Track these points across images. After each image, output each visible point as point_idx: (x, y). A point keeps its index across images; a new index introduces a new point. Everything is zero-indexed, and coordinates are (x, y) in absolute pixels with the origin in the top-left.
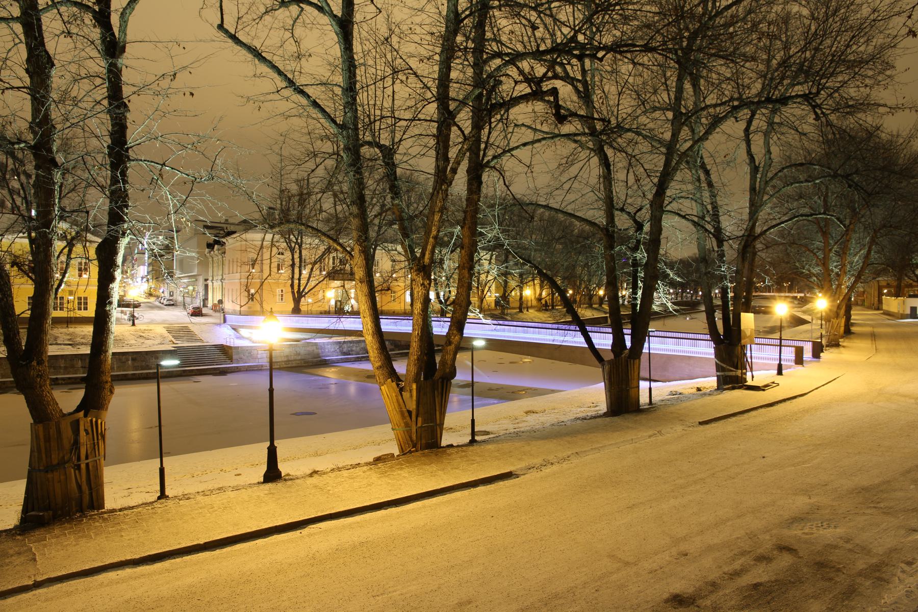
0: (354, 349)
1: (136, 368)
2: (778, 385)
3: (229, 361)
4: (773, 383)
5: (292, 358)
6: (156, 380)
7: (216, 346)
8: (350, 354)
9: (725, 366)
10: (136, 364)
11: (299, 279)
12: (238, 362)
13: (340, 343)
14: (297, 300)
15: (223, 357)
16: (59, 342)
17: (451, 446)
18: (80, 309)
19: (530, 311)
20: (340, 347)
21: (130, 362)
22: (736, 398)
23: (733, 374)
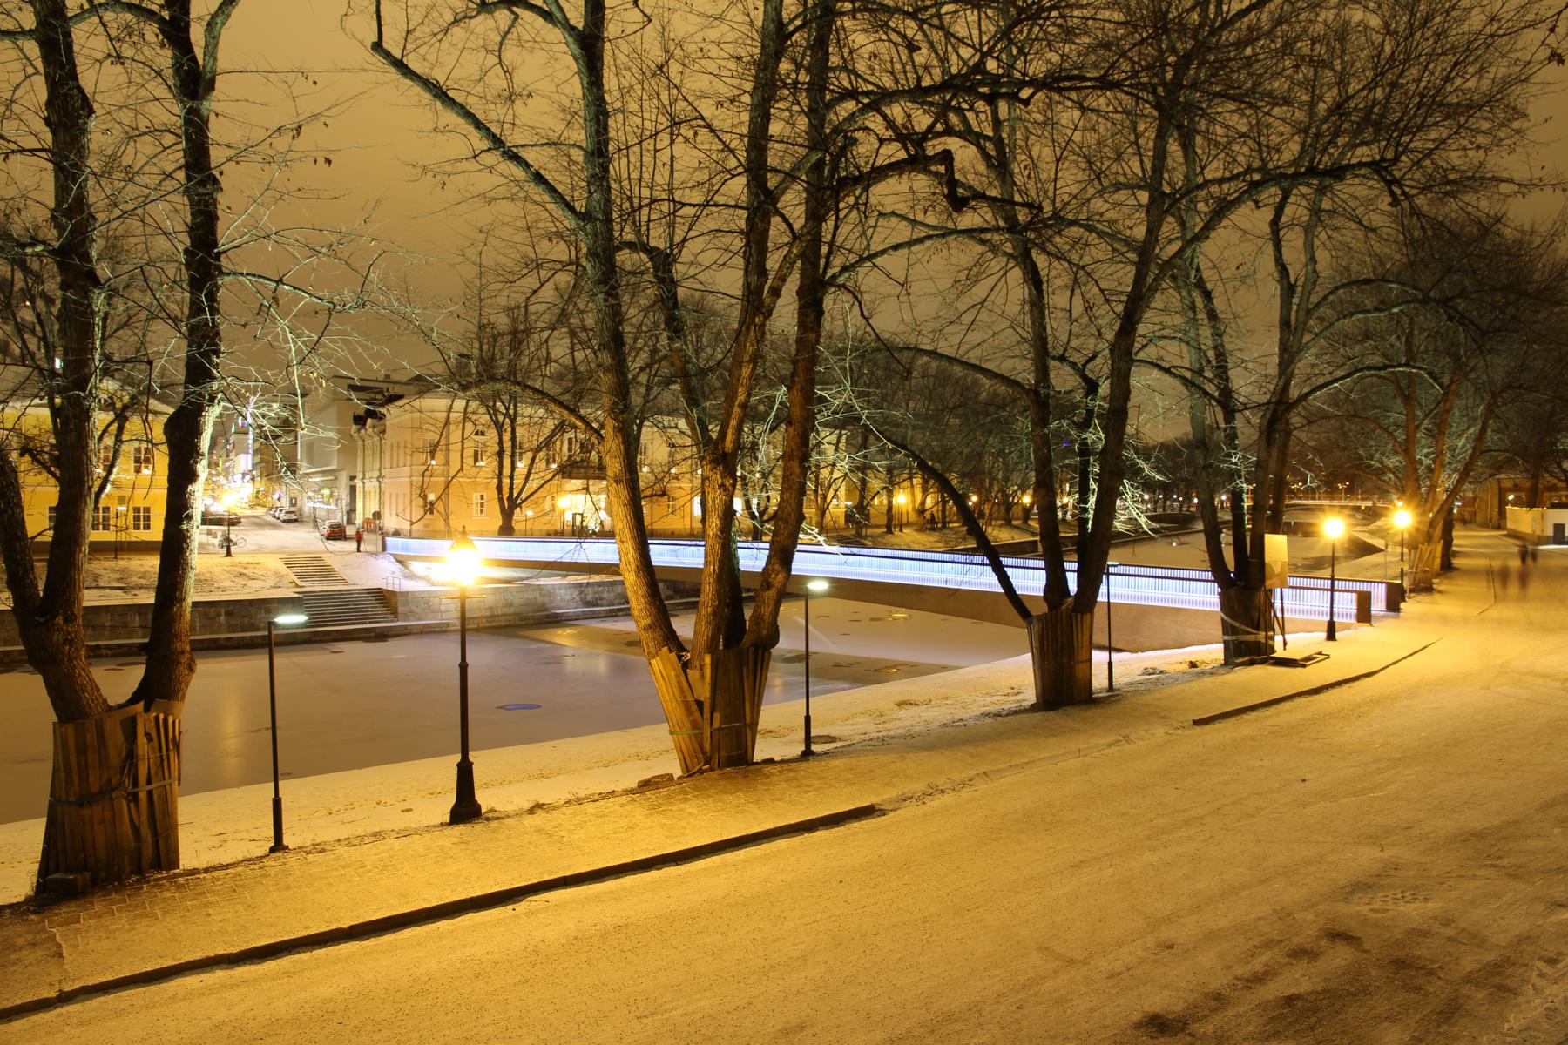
0: (605, 595)
1: (232, 629)
2: (1328, 657)
3: (391, 617)
4: (1320, 653)
5: (500, 612)
6: (267, 649)
7: (369, 591)
8: (597, 605)
9: (1237, 624)
10: (233, 622)
11: (511, 477)
12: (407, 617)
13: (580, 585)
14: (508, 512)
15: (381, 610)
16: (102, 584)
17: (770, 761)
18: (137, 527)
19: (905, 530)
20: (581, 592)
21: (222, 618)
22: (1257, 679)
23: (1251, 638)
